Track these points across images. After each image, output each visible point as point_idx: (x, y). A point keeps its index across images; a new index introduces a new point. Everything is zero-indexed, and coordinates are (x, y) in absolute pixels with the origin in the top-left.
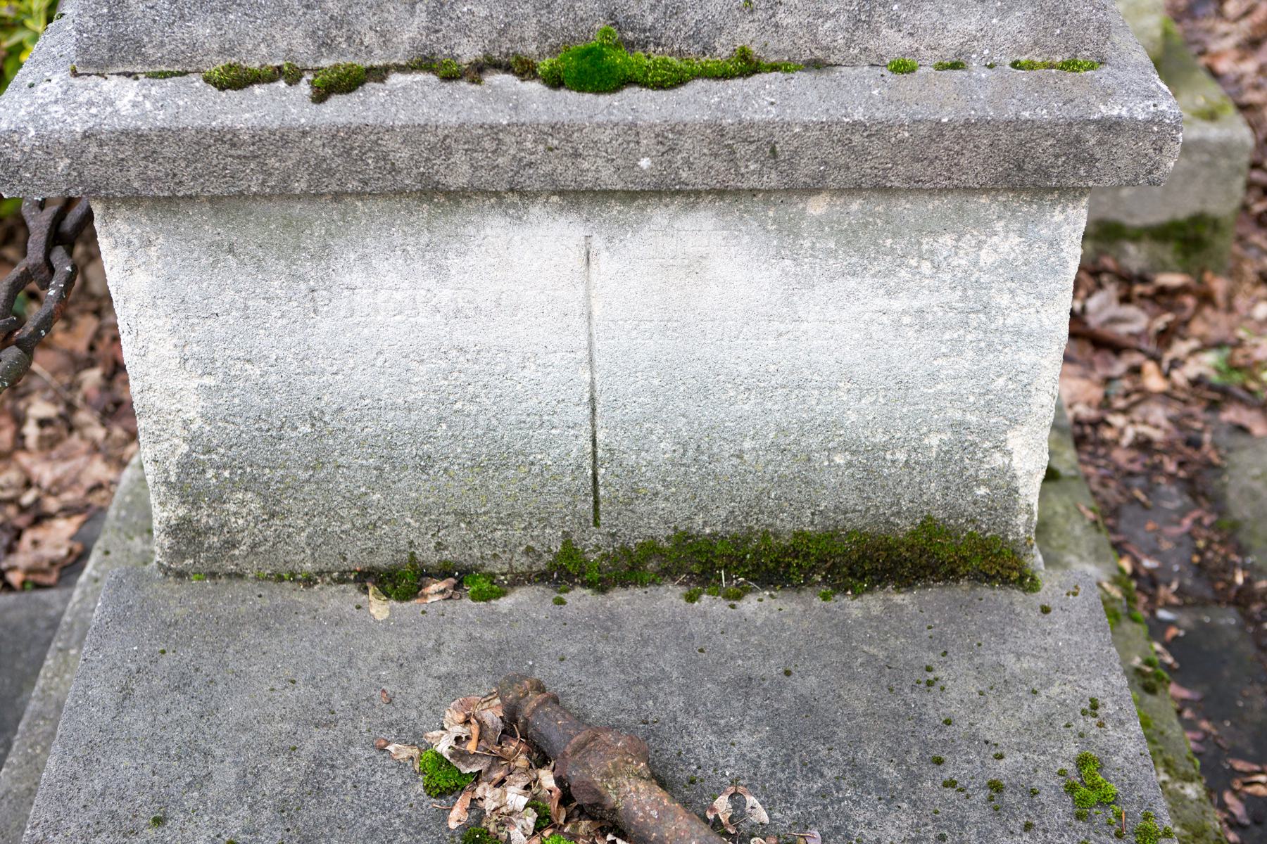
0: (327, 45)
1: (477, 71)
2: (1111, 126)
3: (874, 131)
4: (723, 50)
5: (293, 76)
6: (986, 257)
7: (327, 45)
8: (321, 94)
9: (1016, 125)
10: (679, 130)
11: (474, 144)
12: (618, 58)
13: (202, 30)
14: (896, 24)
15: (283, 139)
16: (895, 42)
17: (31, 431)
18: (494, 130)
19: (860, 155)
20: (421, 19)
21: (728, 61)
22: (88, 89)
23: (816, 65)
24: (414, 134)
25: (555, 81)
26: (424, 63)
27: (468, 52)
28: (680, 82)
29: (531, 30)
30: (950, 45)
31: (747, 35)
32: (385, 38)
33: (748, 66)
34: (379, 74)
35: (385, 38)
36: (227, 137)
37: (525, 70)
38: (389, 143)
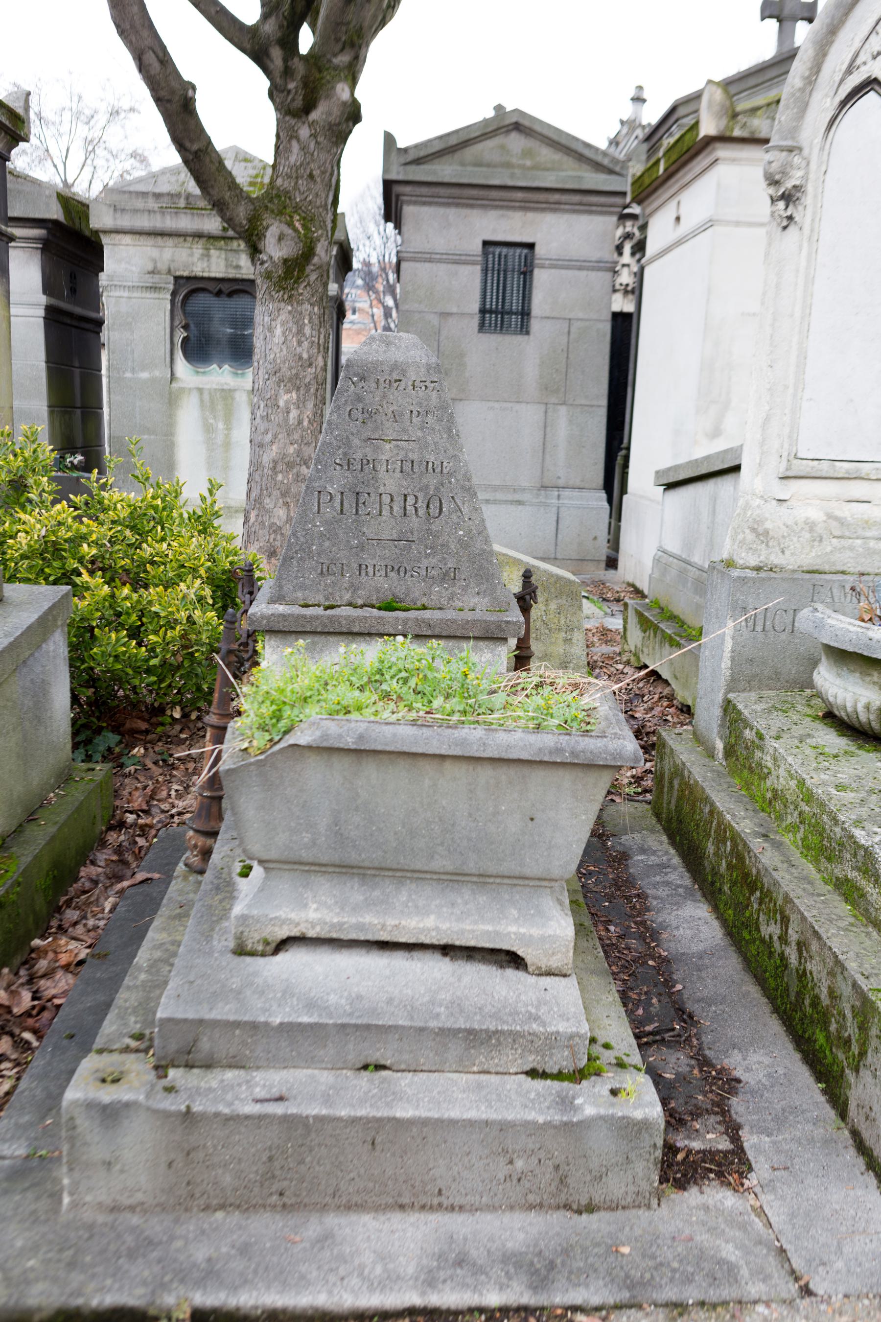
0: (327, 599)
1: (362, 607)
2: (507, 622)
3: (453, 621)
4: (419, 605)
5: (319, 606)
6: (483, 659)
7: (327, 599)
8: (326, 608)
9: (486, 621)
10: (408, 619)
11: (360, 621)
12: (394, 604)
13: (299, 594)
14: (458, 599)
15: (317, 617)
16: (459, 604)
17: (173, 793)
18: (365, 617)
19: (450, 627)
20: (350, 594)
21: (584, 1250)
22: (271, 606)
23: (440, 609)
24: (347, 618)
25: (380, 609)
26: (350, 604)
27: (360, 602)
28: (408, 610)
29: (375, 598)
30: (471, 605)
31: (424, 601)
32: (341, 598)
33: (424, 608)
34: (339, 606)
35: (341, 598)
36: (304, 617)
37: (373, 607)
38: (341, 620)
